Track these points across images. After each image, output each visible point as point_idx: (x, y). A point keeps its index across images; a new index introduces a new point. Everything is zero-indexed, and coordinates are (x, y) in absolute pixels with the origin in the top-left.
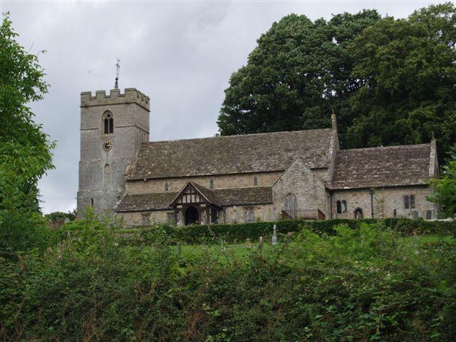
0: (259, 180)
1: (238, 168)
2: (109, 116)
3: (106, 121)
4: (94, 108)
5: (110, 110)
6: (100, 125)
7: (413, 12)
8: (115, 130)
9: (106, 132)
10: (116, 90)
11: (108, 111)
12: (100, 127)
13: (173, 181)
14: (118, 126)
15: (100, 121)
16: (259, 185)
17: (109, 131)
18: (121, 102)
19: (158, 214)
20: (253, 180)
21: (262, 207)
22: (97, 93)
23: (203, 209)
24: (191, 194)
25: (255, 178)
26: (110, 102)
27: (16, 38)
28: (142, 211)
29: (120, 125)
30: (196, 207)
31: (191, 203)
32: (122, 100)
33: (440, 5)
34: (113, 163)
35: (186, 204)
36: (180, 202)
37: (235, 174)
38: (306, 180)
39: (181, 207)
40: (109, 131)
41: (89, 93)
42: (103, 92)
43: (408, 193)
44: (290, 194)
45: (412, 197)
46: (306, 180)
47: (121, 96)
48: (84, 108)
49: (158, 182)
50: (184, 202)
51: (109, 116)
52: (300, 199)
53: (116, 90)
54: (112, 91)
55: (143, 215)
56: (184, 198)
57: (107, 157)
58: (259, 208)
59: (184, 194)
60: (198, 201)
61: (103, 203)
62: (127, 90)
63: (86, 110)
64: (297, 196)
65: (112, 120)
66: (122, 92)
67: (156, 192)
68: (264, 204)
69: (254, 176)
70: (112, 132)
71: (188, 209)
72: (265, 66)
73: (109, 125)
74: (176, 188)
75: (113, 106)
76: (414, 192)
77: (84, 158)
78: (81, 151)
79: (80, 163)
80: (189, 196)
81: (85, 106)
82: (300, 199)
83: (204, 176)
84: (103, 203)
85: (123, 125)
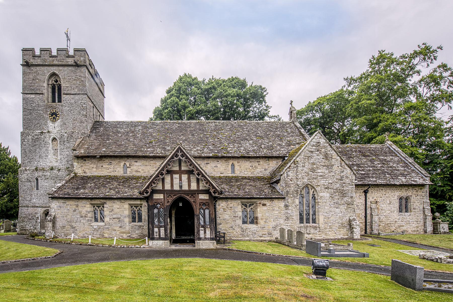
0: (237, 168)
1: (211, 150)
2: (56, 81)
4: (38, 68)
6: (45, 87)
8: (64, 97)
12: (45, 91)
13: (132, 161)
14: (66, 92)
15: (45, 85)
16: (238, 173)
17: (57, 101)
18: (70, 63)
19: (116, 205)
20: (230, 166)
21: (267, 202)
23: (204, 204)
24: (180, 172)
25: (233, 165)
26: (56, 62)
28: (92, 199)
29: (69, 92)
30: (192, 200)
31: (181, 191)
32: (70, 61)
34: (62, 136)
35: (172, 192)
36: (160, 187)
37: (209, 158)
38: (329, 167)
39: (161, 196)
40: (57, 101)
41: (32, 50)
42: (48, 50)
43: (404, 193)
44: (307, 186)
45: (407, 199)
46: (329, 167)
47: (69, 56)
48: (25, 68)
49: (115, 162)
50: (168, 187)
51: (56, 81)
52: (321, 194)
55: (93, 205)
56: (168, 179)
57: (54, 128)
58: (264, 205)
59: (169, 172)
60: (194, 186)
61: (414, 196)
62: (76, 50)
63: (28, 70)
64: (318, 189)
66: (71, 53)
67: (112, 174)
68: (271, 199)
69: (231, 162)
70: (60, 101)
73: (56, 91)
74: (137, 171)
75: (61, 68)
76: (409, 193)
77: (27, 128)
78: (24, 119)
79: (22, 134)
80: (176, 176)
81: (27, 64)
82: (321, 194)
84: (414, 196)
85: (72, 92)
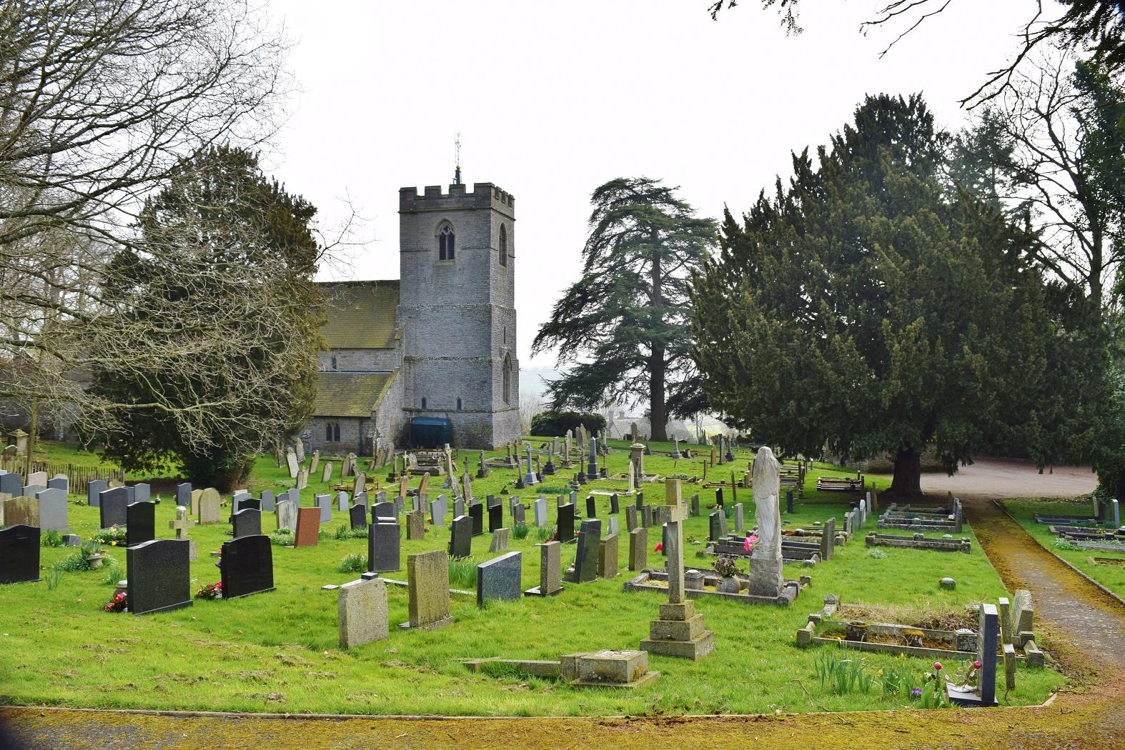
2: (446, 229)
3: (442, 238)
5: (450, 220)
7: (824, 123)
9: (442, 257)
10: (457, 187)
11: (445, 220)
22: (428, 189)
27: (557, 349)
33: (869, 100)
41: (414, 190)
53: (457, 187)
54: (452, 187)
62: (477, 186)
65: (452, 237)
66: (470, 190)
70: (452, 256)
71: (316, 252)
72: (461, 481)
83: (470, 714)
